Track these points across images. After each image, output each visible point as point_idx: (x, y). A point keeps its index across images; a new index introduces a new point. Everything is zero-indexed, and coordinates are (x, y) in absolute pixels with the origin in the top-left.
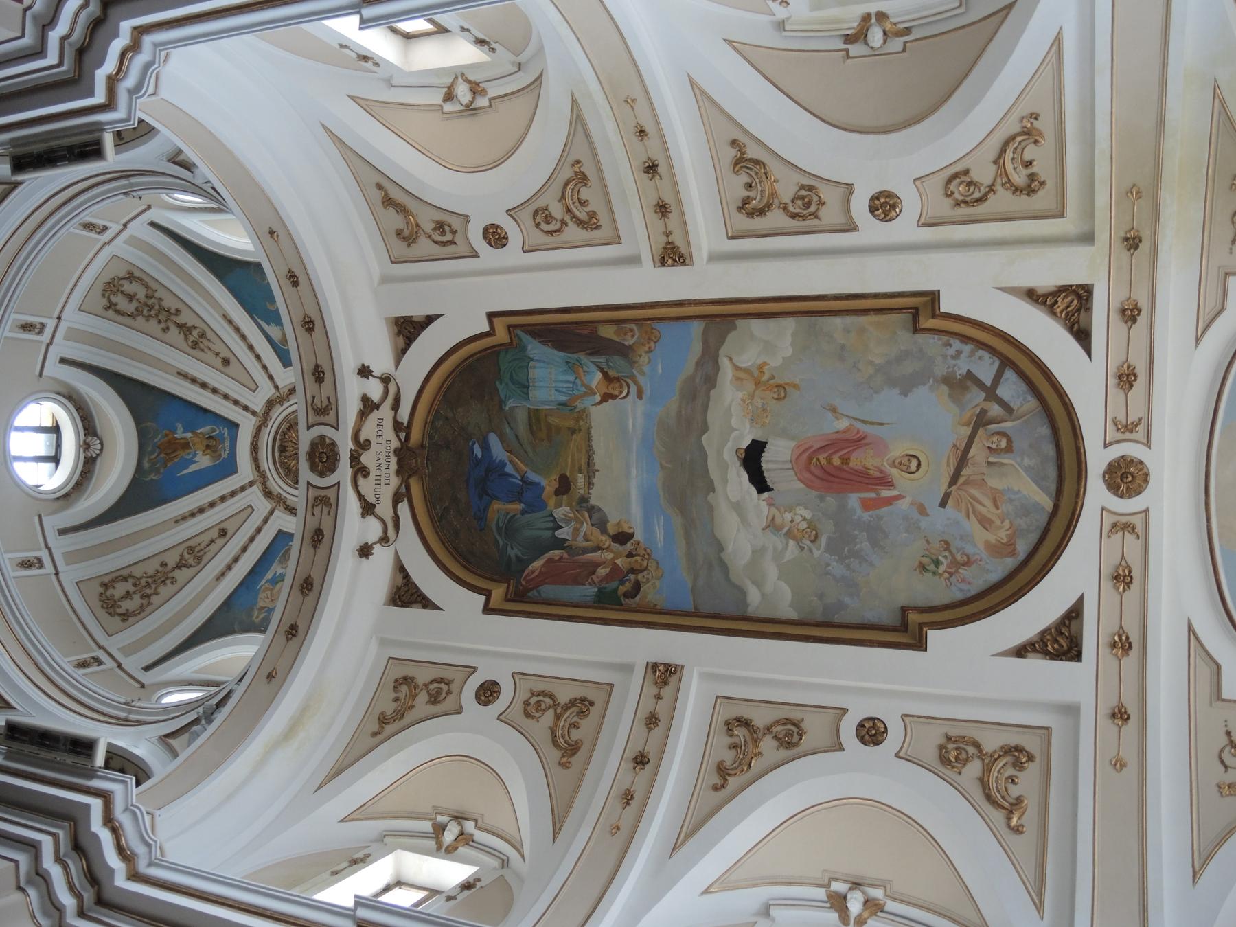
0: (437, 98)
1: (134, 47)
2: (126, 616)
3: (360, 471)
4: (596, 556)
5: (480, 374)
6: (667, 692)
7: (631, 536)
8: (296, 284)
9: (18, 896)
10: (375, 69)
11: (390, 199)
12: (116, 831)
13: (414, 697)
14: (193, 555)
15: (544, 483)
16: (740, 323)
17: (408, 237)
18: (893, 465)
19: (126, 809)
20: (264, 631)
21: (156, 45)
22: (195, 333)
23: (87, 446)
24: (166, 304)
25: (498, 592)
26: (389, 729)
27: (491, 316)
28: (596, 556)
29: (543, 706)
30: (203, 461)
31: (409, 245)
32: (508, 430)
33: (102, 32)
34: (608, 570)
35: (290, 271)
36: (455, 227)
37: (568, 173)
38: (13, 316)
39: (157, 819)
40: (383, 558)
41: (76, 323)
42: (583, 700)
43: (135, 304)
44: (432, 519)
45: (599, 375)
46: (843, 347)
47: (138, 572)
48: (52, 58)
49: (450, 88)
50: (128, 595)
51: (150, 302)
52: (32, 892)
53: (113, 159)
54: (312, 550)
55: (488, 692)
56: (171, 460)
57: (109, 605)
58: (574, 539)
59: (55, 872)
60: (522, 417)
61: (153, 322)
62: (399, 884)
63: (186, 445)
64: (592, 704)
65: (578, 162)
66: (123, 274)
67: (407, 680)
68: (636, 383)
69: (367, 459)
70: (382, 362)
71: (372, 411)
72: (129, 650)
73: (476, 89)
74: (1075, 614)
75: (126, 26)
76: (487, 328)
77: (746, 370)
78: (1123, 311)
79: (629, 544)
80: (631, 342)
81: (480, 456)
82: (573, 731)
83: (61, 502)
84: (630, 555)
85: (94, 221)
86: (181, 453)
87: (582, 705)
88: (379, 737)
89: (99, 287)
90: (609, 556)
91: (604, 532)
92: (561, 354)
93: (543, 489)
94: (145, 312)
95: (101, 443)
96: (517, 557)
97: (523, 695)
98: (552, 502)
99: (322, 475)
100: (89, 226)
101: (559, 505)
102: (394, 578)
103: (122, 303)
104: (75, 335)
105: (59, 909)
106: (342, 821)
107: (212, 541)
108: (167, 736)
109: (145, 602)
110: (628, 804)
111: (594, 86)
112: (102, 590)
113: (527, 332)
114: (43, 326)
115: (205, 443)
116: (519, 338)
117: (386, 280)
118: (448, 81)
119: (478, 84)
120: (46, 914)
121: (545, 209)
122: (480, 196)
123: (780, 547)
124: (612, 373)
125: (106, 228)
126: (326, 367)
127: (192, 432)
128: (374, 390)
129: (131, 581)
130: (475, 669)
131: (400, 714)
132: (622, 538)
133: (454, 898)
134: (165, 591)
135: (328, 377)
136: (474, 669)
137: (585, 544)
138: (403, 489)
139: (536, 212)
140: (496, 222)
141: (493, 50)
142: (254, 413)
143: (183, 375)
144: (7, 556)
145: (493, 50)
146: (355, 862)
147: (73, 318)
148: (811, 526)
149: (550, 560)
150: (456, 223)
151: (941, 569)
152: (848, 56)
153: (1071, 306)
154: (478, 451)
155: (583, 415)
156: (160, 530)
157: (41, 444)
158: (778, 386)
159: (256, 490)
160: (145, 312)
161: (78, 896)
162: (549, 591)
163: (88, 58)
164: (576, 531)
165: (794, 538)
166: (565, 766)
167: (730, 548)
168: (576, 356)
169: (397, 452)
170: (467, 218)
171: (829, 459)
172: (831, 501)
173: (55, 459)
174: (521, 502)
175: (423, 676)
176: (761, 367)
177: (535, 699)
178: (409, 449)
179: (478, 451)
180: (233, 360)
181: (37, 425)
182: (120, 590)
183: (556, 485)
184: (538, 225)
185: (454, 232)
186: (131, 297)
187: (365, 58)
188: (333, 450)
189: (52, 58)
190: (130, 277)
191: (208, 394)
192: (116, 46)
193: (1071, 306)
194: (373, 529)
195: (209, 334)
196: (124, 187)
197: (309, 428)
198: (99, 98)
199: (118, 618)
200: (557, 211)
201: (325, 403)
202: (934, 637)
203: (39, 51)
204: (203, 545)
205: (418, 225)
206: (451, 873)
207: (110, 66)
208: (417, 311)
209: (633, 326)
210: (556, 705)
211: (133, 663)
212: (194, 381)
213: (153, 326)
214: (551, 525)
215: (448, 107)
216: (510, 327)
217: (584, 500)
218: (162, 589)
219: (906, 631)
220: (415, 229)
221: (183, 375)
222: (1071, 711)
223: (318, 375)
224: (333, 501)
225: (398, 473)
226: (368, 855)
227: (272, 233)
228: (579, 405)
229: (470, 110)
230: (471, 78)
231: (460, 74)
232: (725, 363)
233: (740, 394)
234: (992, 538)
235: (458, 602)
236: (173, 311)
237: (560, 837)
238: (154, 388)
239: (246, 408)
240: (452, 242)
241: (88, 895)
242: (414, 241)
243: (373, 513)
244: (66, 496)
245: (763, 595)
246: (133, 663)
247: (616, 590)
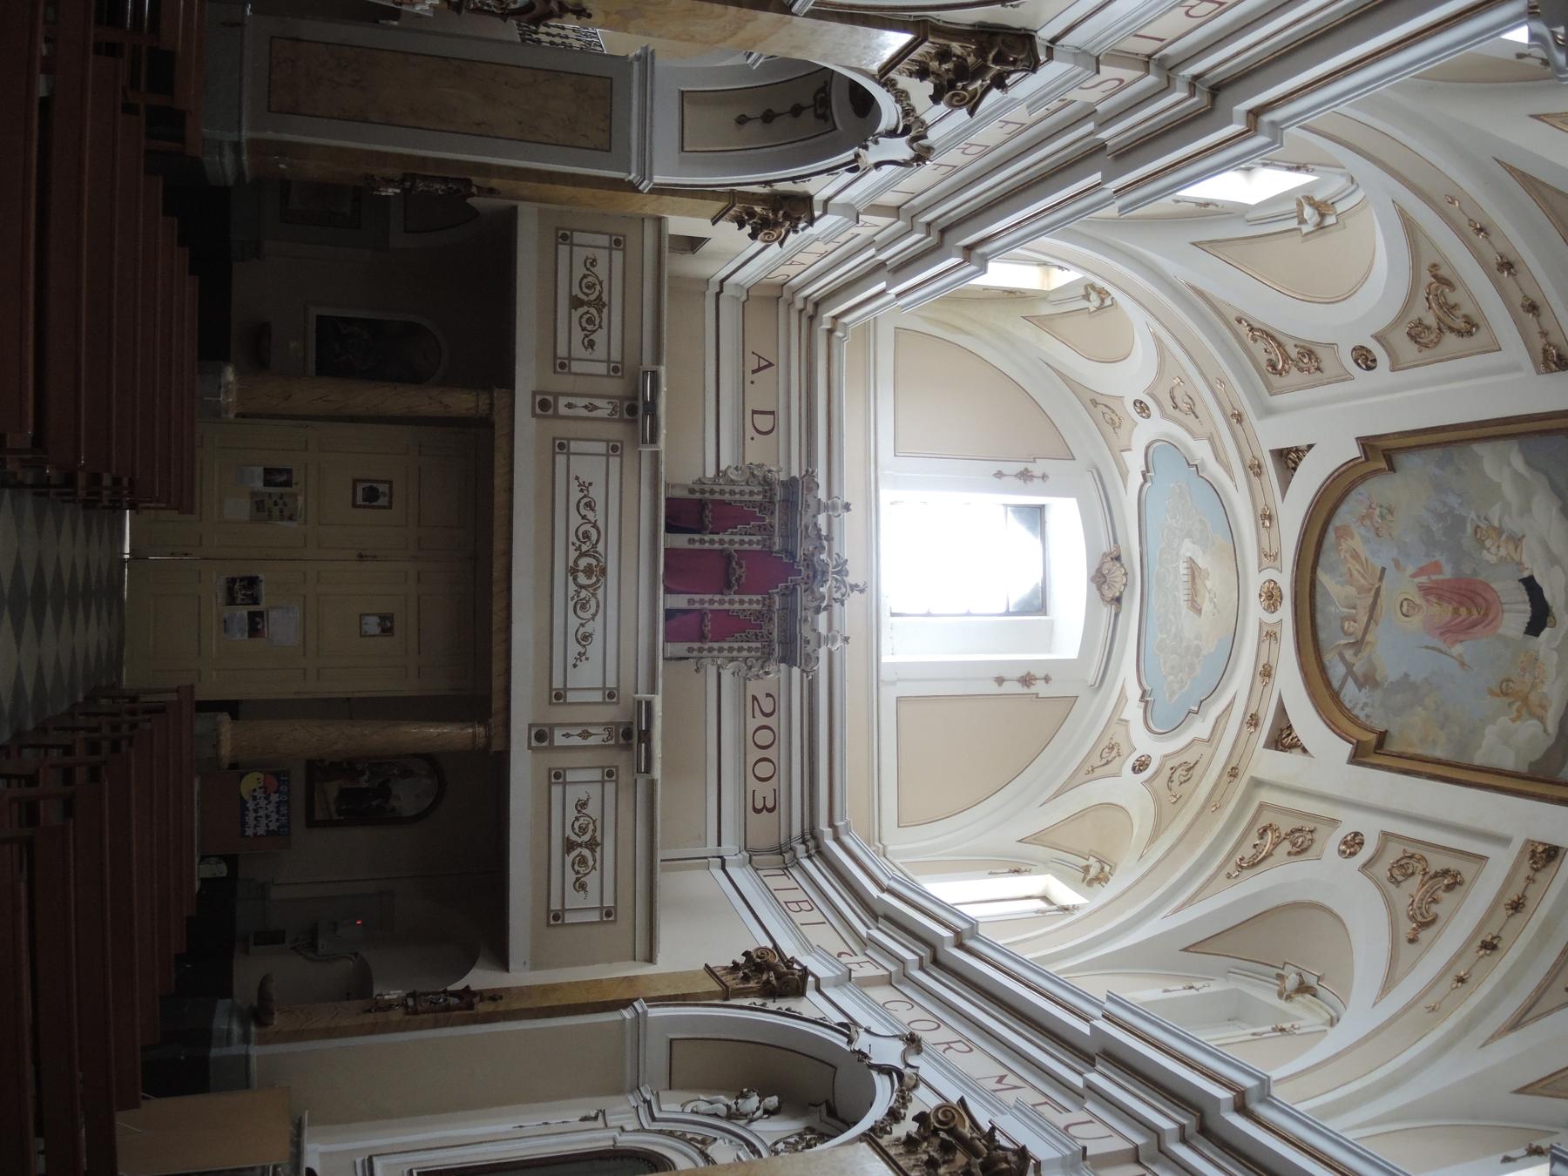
6: (1539, 343)
16: (1524, 769)
18: (1420, 607)
46: (1442, 727)
74: (1285, 484)
77: (1532, 715)
78: (1256, 725)
123: (1506, 518)
148: (1481, 543)
151: (1377, 512)
152: (1319, 978)
153: (1283, 738)
158: (1506, 695)
165: (1494, 528)
167: (1555, 512)
171: (1470, 613)
172: (1467, 570)
176: (1519, 717)
193: (1283, 738)
202: (1355, 452)
219: (1381, 453)
222: (1267, 412)
230: (1318, 198)
232: (1552, 727)
233: (1545, 689)
234: (1350, 542)
245: (1510, 465)
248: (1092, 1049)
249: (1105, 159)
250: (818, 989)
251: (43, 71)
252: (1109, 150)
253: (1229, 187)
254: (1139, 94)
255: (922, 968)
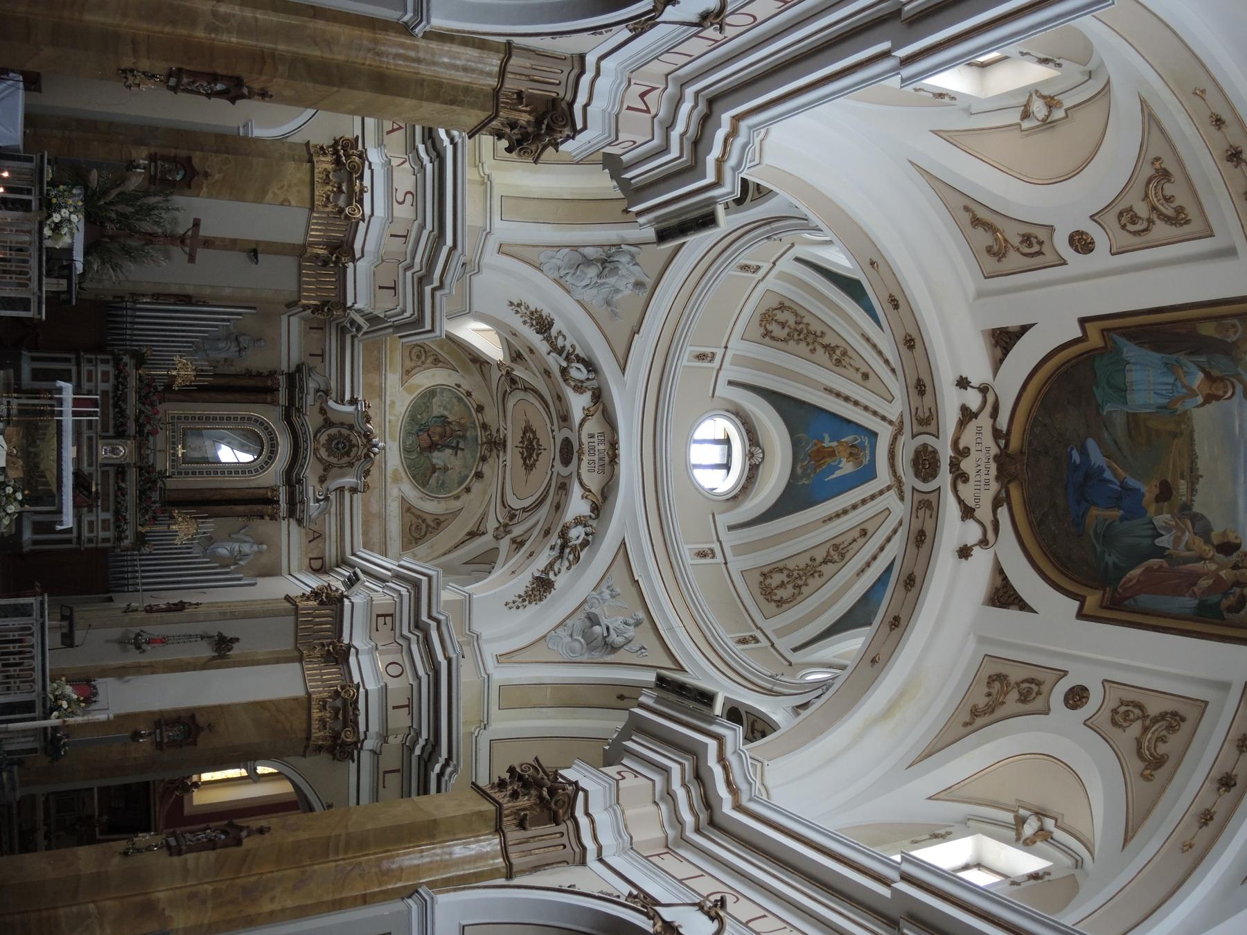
0: (1014, 117)
1: (734, 133)
2: (780, 603)
3: (960, 476)
4: (1198, 566)
5: (1078, 379)
7: (1238, 546)
8: (896, 307)
9: (653, 808)
10: (953, 102)
11: (977, 219)
12: (726, 768)
13: (1006, 694)
14: (838, 552)
15: (1144, 489)
17: (998, 252)
19: (735, 752)
20: (870, 624)
21: (750, 128)
22: (838, 352)
23: (751, 455)
24: (812, 328)
25: (1093, 599)
26: (979, 721)
27: (1083, 321)
28: (1198, 566)
29: (1132, 716)
30: (847, 467)
31: (999, 260)
32: (1106, 435)
33: (711, 122)
34: (1211, 582)
35: (891, 296)
36: (1041, 238)
37: (1148, 171)
38: (689, 349)
39: (766, 768)
40: (982, 560)
41: (740, 350)
42: (1174, 714)
43: (787, 330)
44: (1030, 523)
45: (1201, 375)
47: (791, 565)
48: (674, 152)
49: (1027, 106)
50: (782, 585)
51: (799, 327)
52: (663, 807)
53: (726, 221)
54: (916, 551)
55: (1076, 697)
56: (820, 466)
57: (767, 592)
58: (1175, 547)
59: (681, 793)
60: (1120, 420)
61: (803, 344)
62: (979, 866)
63: (832, 453)
64: (1183, 719)
65: (1157, 159)
66: (775, 305)
67: (1000, 678)
68: (1241, 381)
69: (966, 465)
70: (979, 372)
71: (970, 419)
72: (783, 632)
73: (1051, 103)
75: (726, 117)
76: (1079, 334)
79: (1235, 555)
80: (1234, 338)
81: (1078, 462)
82: (1160, 744)
83: (730, 503)
84: (1236, 567)
85: (748, 263)
86: (828, 460)
87: (1172, 720)
88: (970, 728)
89: (757, 318)
90: (1213, 567)
91: (1208, 541)
92: (1159, 356)
93: (1143, 495)
94: (796, 337)
95: (763, 452)
96: (1114, 563)
97: (1112, 704)
98: (1152, 509)
99: (925, 480)
100: (745, 268)
101: (1159, 512)
102: (993, 578)
103: (774, 328)
104: (740, 361)
105: (681, 823)
106: (929, 798)
107: (854, 540)
108: (798, 707)
109: (796, 591)
110: (1206, 824)
111: (1157, 84)
112: (761, 579)
113: (1123, 335)
114: (713, 354)
115: (849, 450)
116: (1115, 343)
117: (980, 294)
118: (1023, 100)
119: (1052, 98)
120: (672, 826)
121: (1130, 209)
122: (1063, 206)
124: (1215, 373)
125: (759, 268)
126: (927, 381)
127: (838, 441)
128: (973, 399)
129: (786, 572)
130: (1065, 673)
131: (990, 709)
132: (1228, 548)
133: (1019, 884)
134: (814, 582)
135: (929, 389)
136: (1065, 673)
137: (1188, 553)
138: (1003, 495)
139: (1121, 214)
140: (1082, 229)
141: (1059, 65)
142: (891, 423)
143: (829, 390)
144: (686, 547)
145: (1059, 65)
146: (935, 836)
147: (737, 346)
149: (1149, 570)
150: (1042, 234)
154: (1076, 457)
155: (1185, 417)
156: (810, 529)
157: (715, 454)
159: (893, 494)
160: (796, 337)
161: (696, 816)
162: (1145, 600)
163: (701, 147)
164: (1177, 540)
166: (1147, 778)
168: (1175, 356)
169: (997, 458)
170: (1051, 228)
173: (727, 466)
174: (1120, 508)
175: (1015, 675)
177: (1123, 709)
178: (1008, 455)
179: (1076, 457)
180: (872, 375)
181: (712, 437)
182: (777, 579)
183: (1156, 491)
184: (1124, 227)
185: (1041, 243)
186: (783, 325)
187: (941, 95)
188: (934, 457)
189: (674, 152)
190: (782, 307)
191: (850, 406)
192: (720, 135)
194: (972, 532)
195: (851, 353)
196: (768, 232)
197: (913, 437)
198: (710, 178)
199: (773, 604)
200: (1142, 210)
201: (927, 414)
203: (665, 149)
204: (846, 543)
205: (1005, 240)
206: (1025, 862)
207: (716, 151)
208: (1012, 322)
209: (1236, 322)
210: (1145, 716)
211: (784, 644)
212: (838, 395)
213: (803, 348)
214: (1150, 532)
215: (1026, 125)
216: (1103, 331)
217: (1186, 507)
218: (810, 581)
220: (1004, 244)
221: (829, 390)
223: (920, 387)
224: (934, 504)
225: (997, 478)
226: (949, 833)
227: (872, 263)
228: (1180, 408)
229: (1047, 124)
230: (1045, 93)
231: (1034, 91)
235: (1053, 605)
236: (818, 333)
237: (1130, 845)
238: (804, 403)
239: (884, 418)
240: (1040, 253)
241: (703, 817)
242: (1004, 256)
243: (973, 517)
244: (735, 497)
246: (784, 644)
247: (1219, 603)
248: (894, 912)
249: (895, 26)
250: (601, 860)
251: (214, 890)
252: (904, 16)
253: (953, 80)
254: (757, 38)
255: (698, 830)
